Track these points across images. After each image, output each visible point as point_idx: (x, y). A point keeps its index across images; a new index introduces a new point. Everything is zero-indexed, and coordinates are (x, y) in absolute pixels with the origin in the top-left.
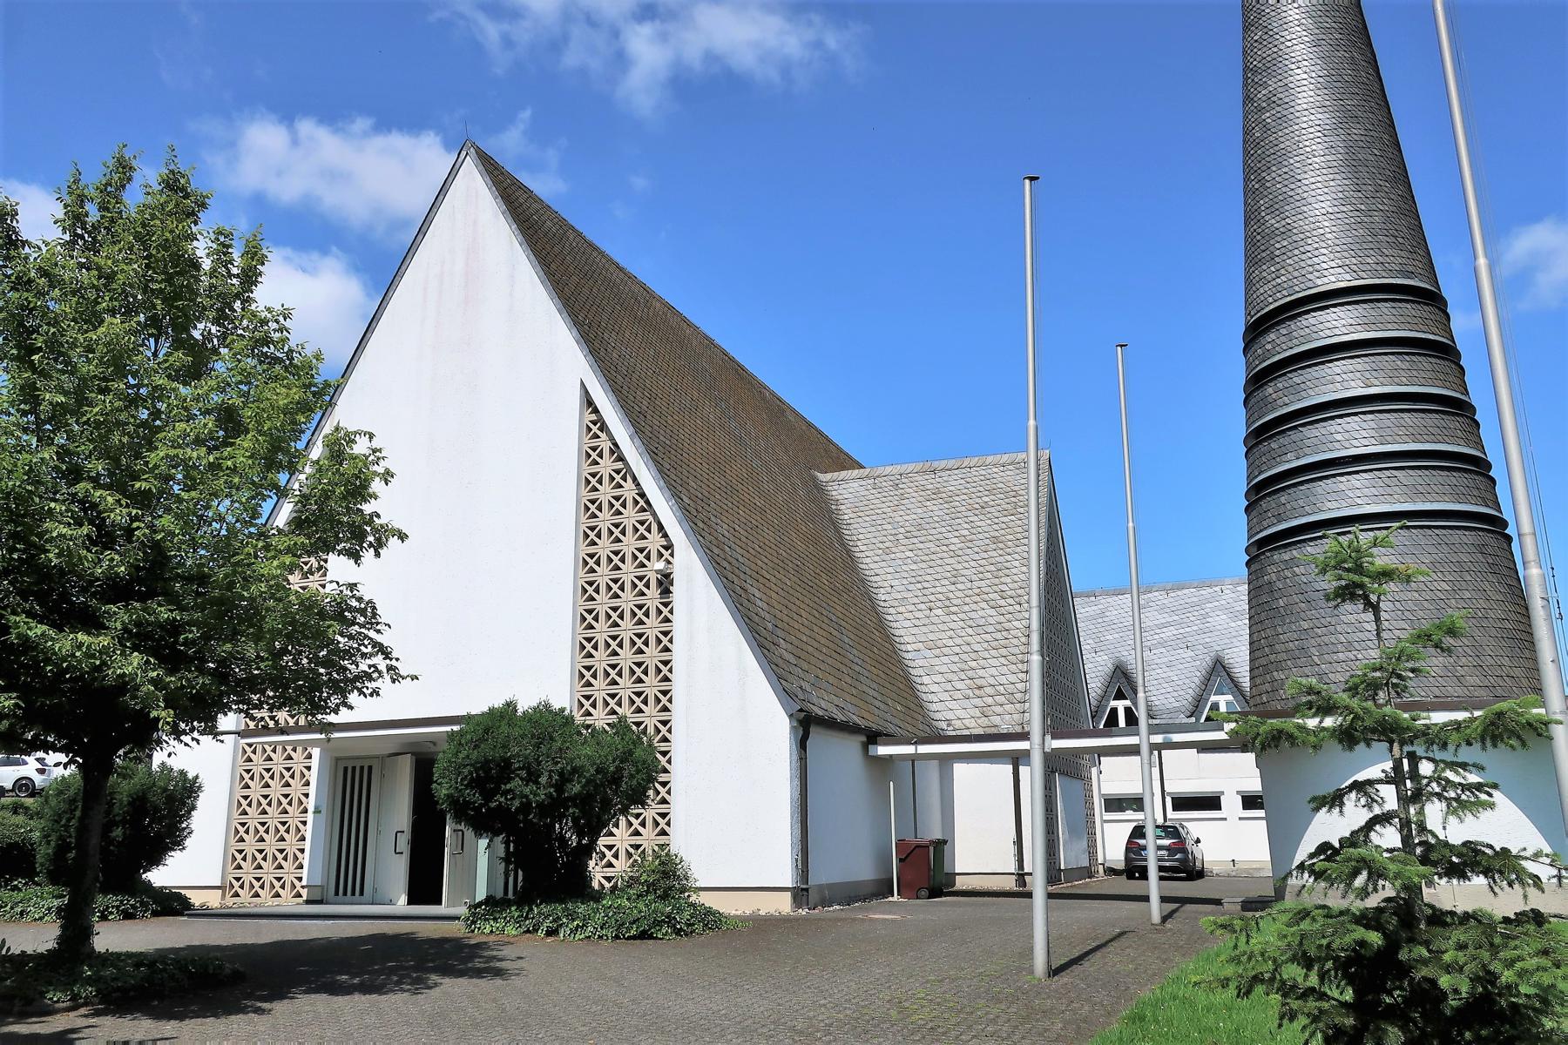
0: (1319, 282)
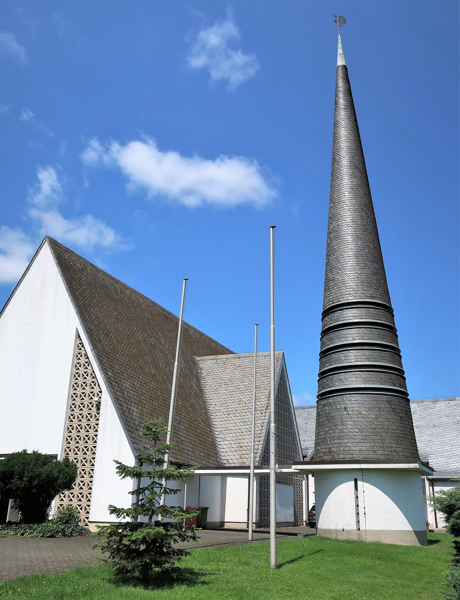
0: (341, 300)
